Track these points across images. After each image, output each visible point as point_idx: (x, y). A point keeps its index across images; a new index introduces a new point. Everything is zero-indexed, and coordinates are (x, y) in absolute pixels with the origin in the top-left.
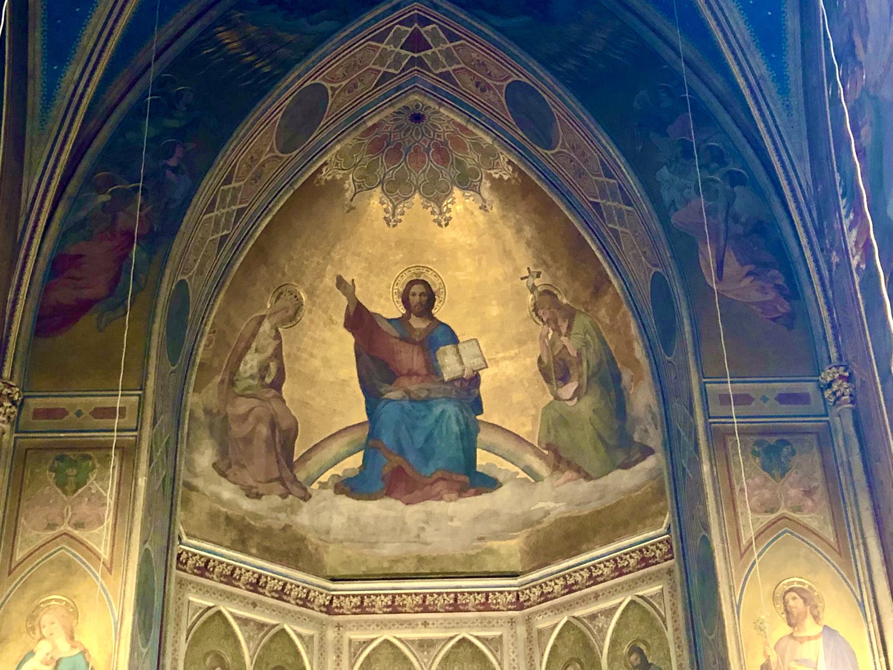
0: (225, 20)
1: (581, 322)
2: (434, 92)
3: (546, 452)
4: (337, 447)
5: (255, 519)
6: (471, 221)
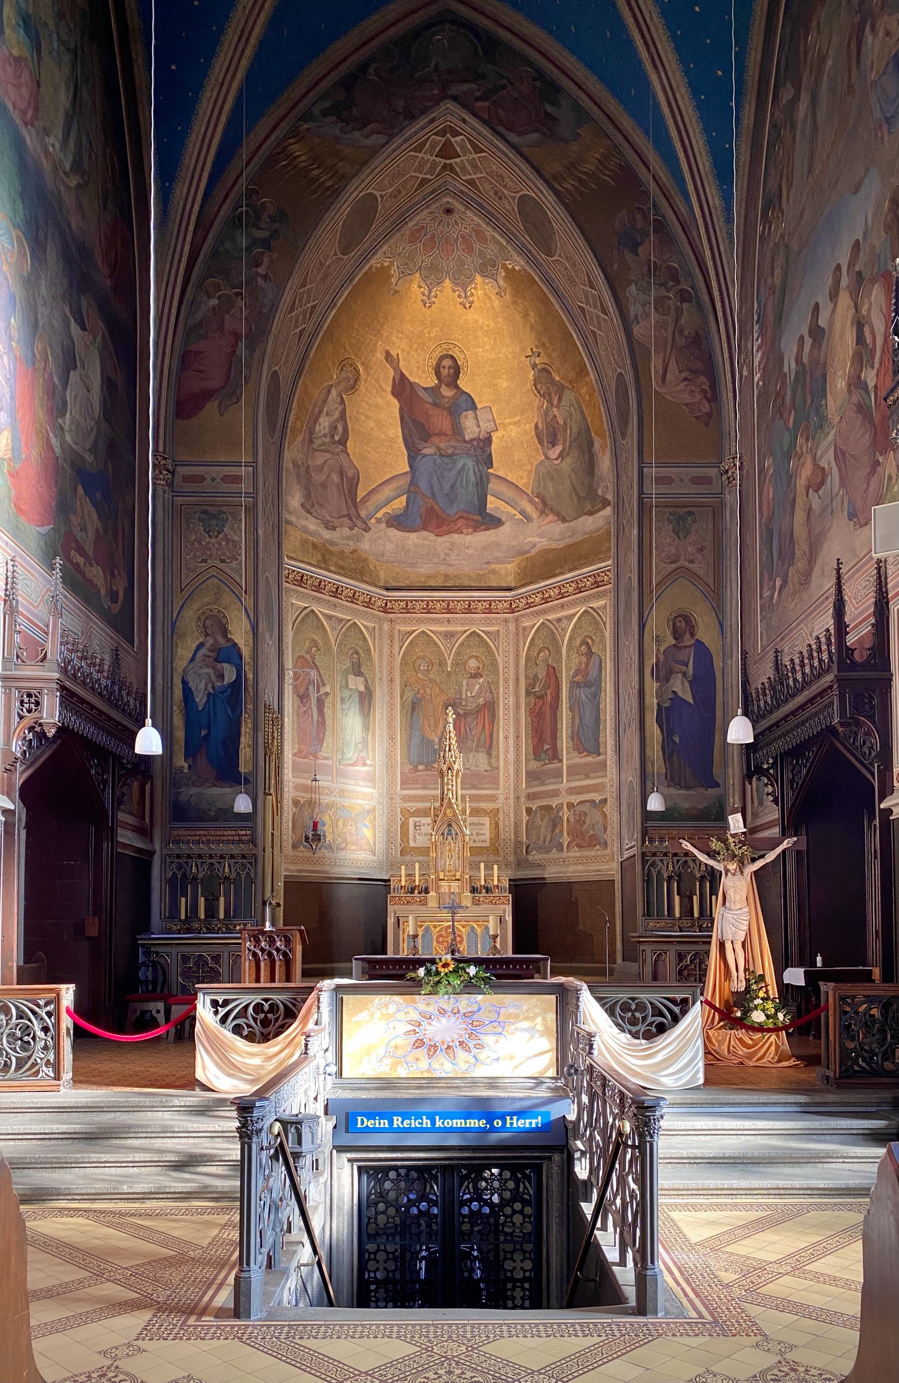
0: (294, 133)
1: (568, 396)
2: (460, 196)
3: (536, 500)
4: (387, 492)
5: (332, 545)
6: (488, 305)
